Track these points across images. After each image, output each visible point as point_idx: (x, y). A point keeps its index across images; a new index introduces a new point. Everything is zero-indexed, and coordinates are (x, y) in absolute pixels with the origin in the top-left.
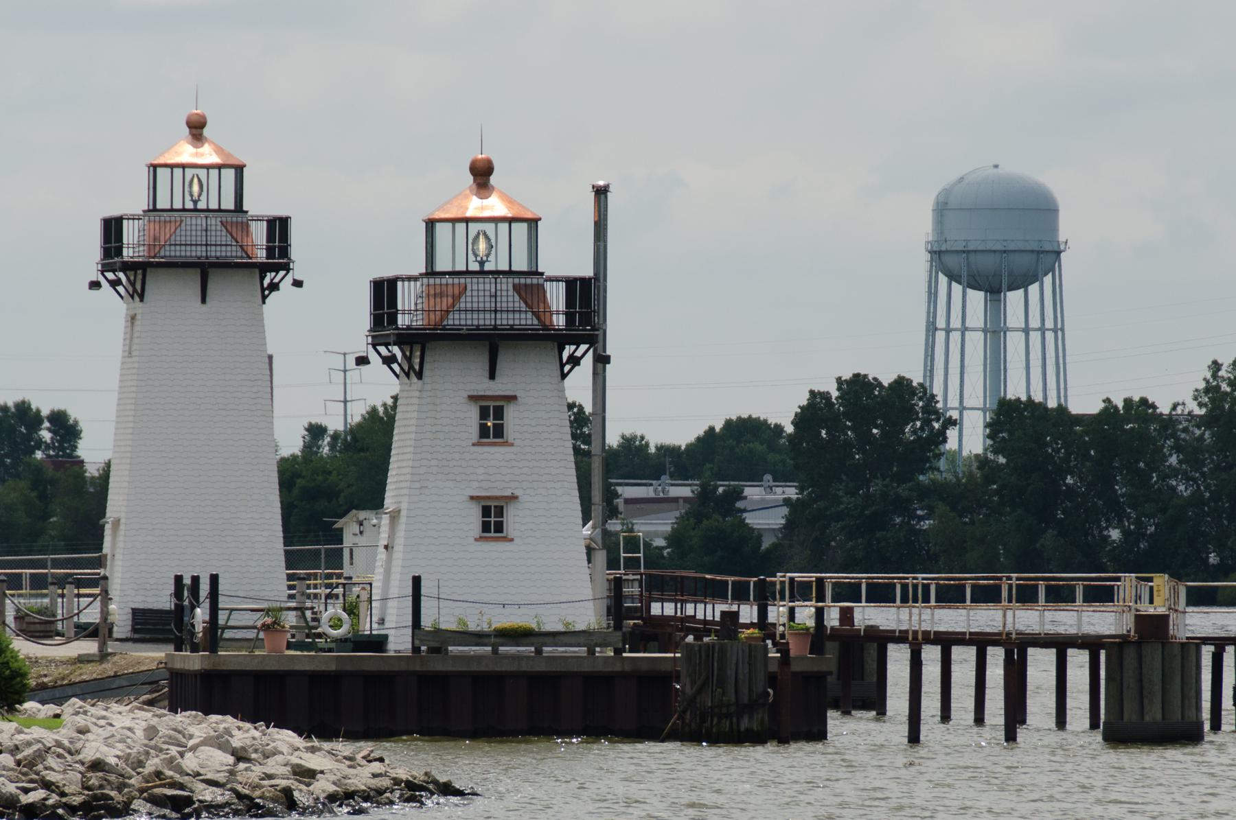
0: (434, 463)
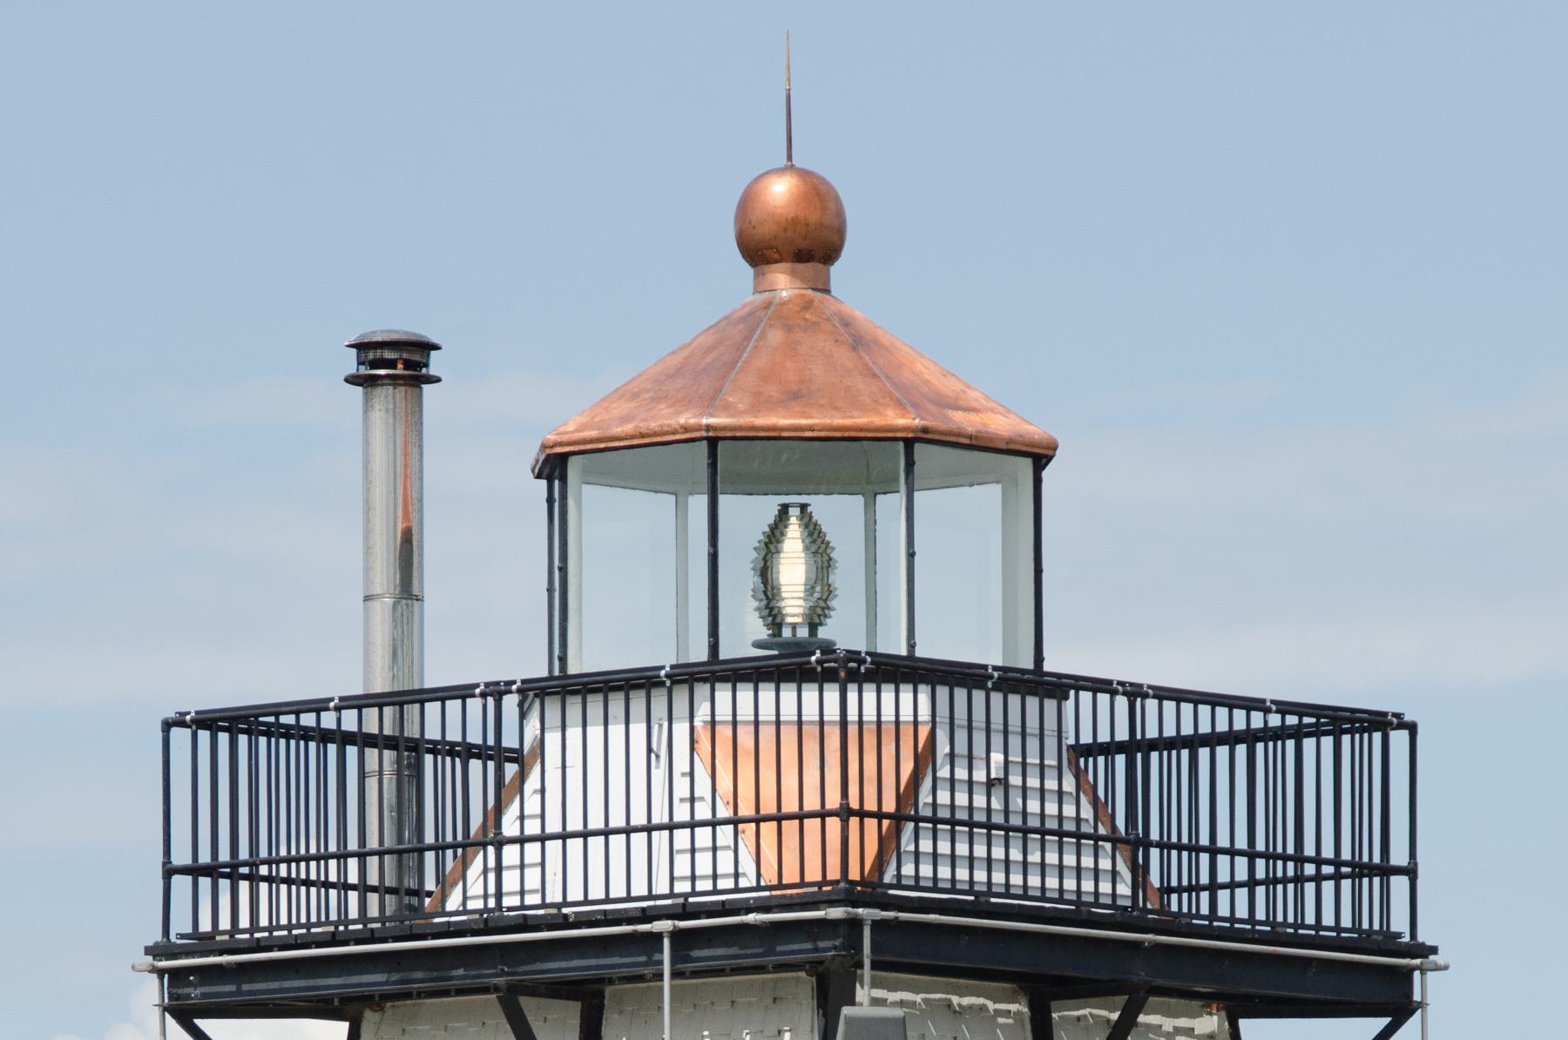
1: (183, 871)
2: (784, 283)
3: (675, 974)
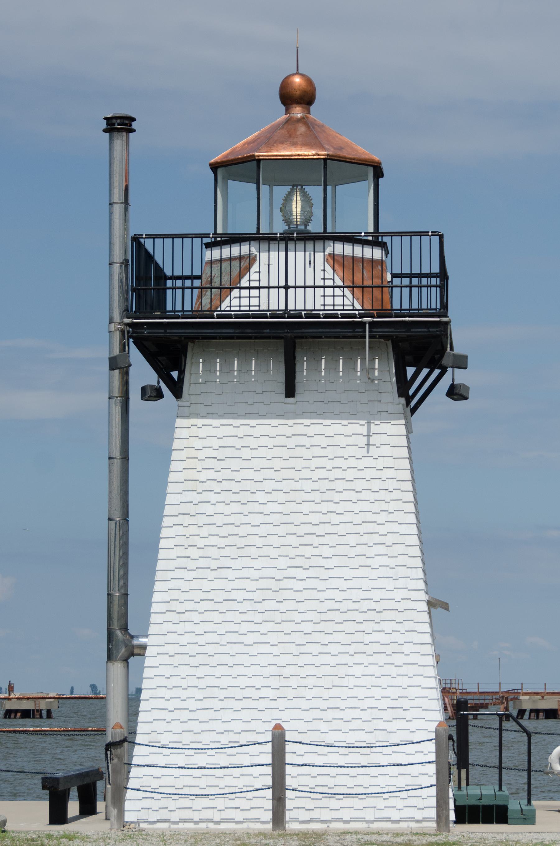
2: (298, 112)
3: (370, 337)
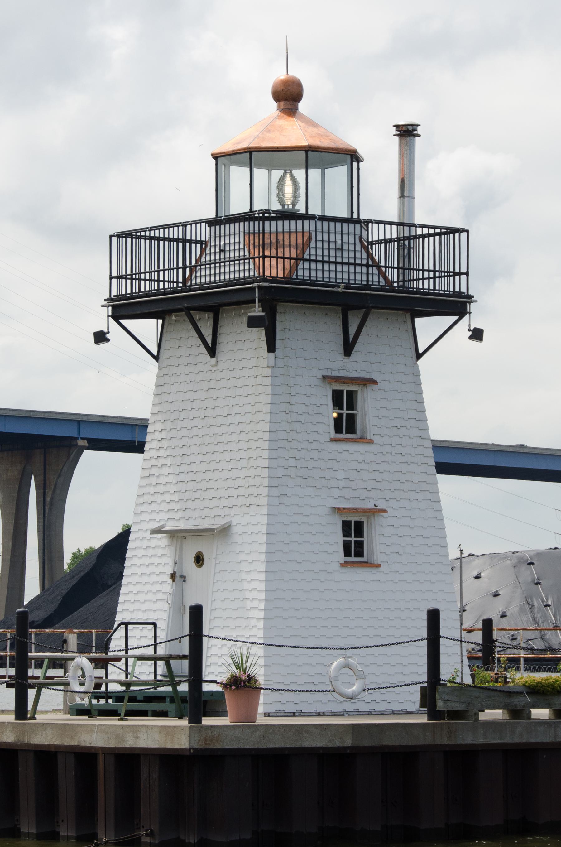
0: (292, 462)
1: (463, 274)
